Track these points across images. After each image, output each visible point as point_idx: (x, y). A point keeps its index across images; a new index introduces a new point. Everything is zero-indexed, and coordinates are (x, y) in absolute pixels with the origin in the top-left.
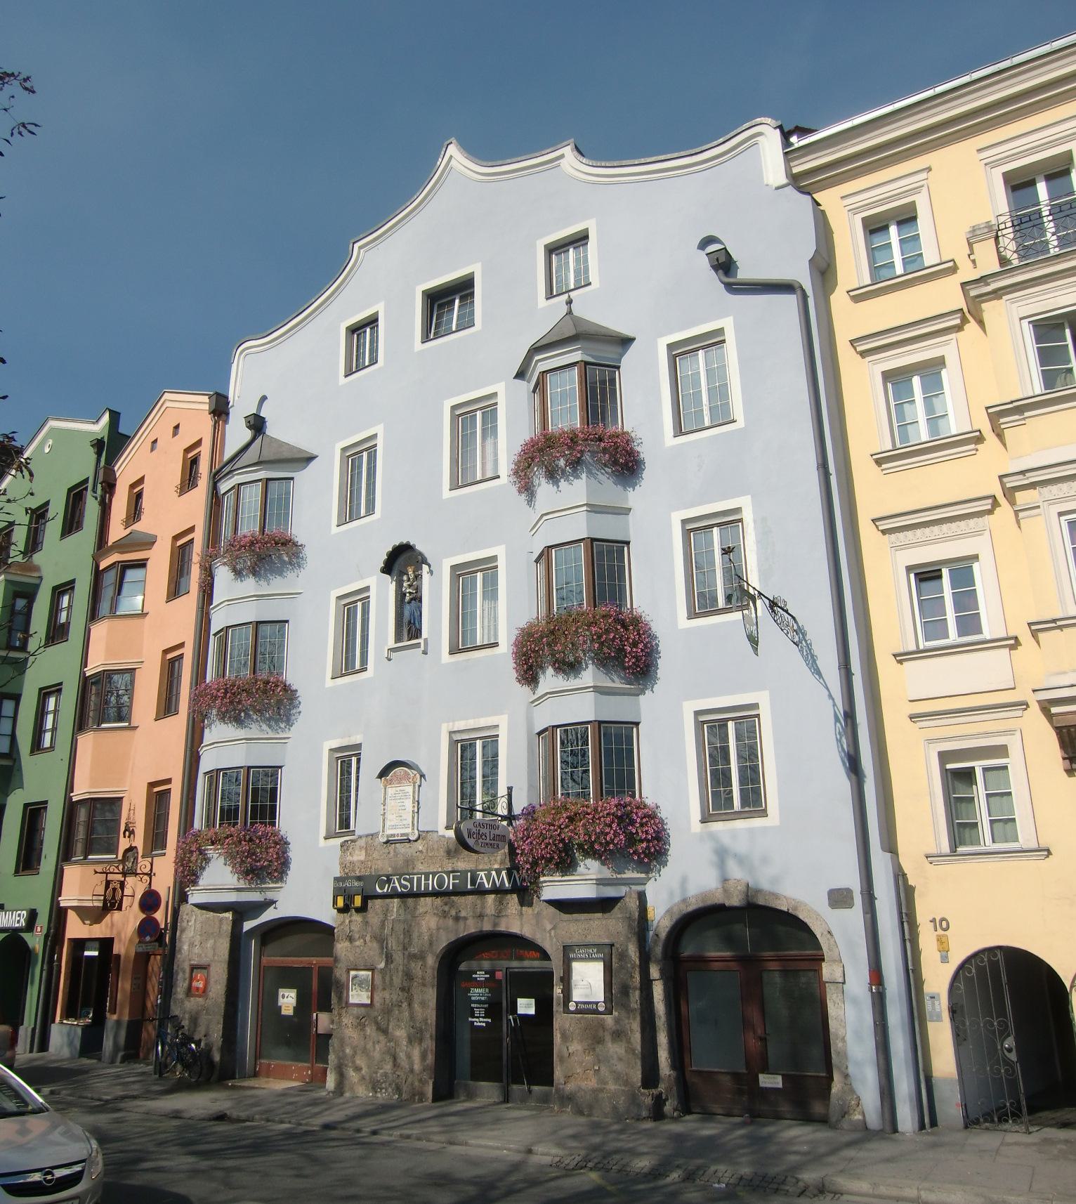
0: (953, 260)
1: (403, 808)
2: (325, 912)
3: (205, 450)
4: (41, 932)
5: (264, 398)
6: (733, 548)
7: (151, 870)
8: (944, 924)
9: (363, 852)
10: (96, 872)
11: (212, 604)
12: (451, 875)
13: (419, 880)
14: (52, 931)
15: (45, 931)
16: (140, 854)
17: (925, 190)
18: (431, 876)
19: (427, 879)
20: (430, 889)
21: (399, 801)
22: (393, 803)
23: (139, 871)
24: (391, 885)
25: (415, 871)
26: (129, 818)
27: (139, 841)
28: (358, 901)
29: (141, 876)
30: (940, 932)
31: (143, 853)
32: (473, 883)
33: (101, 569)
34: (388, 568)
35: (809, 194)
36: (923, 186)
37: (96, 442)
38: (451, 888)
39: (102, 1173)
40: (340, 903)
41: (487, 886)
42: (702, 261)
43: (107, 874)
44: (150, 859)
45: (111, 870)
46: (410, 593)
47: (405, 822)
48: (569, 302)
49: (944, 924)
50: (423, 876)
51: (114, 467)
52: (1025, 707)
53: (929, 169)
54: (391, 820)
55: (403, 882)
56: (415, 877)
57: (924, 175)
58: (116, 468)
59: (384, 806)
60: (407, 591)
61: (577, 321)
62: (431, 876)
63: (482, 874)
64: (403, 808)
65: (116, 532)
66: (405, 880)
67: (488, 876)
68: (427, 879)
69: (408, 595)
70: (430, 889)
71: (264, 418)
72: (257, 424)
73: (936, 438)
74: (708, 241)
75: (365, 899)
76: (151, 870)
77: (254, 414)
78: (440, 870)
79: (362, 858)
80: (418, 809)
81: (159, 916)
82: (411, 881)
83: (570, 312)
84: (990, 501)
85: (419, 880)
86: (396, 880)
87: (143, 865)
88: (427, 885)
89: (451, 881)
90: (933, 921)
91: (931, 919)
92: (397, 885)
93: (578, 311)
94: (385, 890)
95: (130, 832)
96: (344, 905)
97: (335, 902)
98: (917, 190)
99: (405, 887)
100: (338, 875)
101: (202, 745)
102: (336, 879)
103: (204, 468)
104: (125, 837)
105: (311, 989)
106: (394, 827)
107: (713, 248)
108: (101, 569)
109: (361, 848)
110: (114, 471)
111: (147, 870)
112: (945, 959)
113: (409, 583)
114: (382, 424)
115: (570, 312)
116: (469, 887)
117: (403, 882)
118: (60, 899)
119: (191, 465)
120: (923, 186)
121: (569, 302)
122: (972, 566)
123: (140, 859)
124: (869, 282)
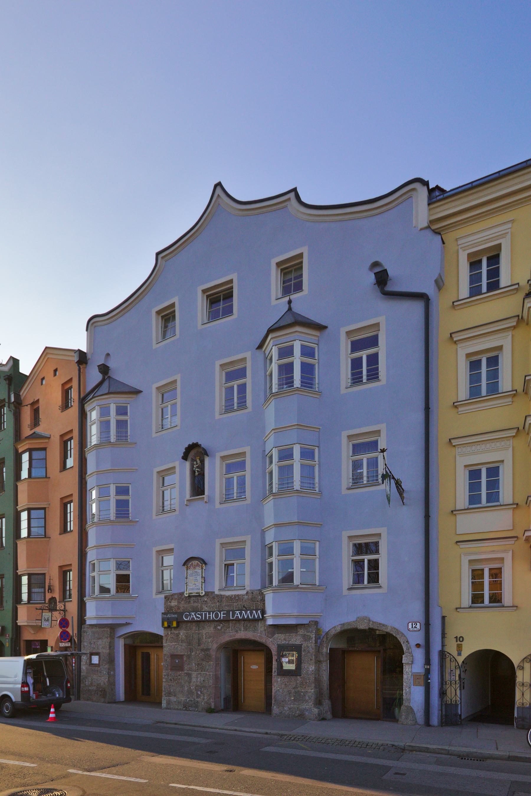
0: (518, 284)
1: (197, 580)
2: (159, 630)
3: (75, 384)
4: (8, 637)
5: (108, 355)
6: (386, 450)
7: (65, 608)
8: (461, 639)
9: (176, 601)
10: (37, 609)
11: (87, 474)
12: (222, 612)
13: (206, 615)
14: (14, 636)
15: (11, 636)
16: (58, 600)
17: (509, 236)
18: (211, 613)
19: (210, 614)
20: (211, 619)
21: (194, 577)
22: (191, 578)
23: (58, 609)
24: (191, 617)
25: (203, 610)
26: (50, 583)
27: (57, 595)
28: (175, 624)
29: (60, 611)
30: (459, 643)
31: (59, 599)
32: (233, 616)
33: (20, 452)
34: (185, 457)
35: (440, 234)
36: (508, 233)
37: (7, 377)
38: (222, 618)
39: (381, 633)
40: (166, 624)
41: (240, 618)
42: (372, 278)
43: (42, 610)
44: (63, 603)
45: (44, 608)
46: (197, 471)
47: (197, 587)
48: (290, 302)
49: (461, 639)
50: (208, 613)
51: (19, 393)
52: (516, 539)
53: (512, 221)
54: (191, 586)
55: (197, 615)
56: (204, 613)
57: (510, 225)
58: (21, 394)
59: (187, 579)
60: (196, 470)
61: (295, 314)
62: (211, 613)
63: (238, 612)
64: (197, 580)
65: (27, 431)
66: (198, 614)
67: (241, 614)
68: (210, 614)
69: (196, 472)
70: (211, 619)
71: (109, 367)
72: (104, 369)
73: (493, 394)
74: (376, 264)
75: (178, 623)
76: (65, 608)
77: (103, 364)
78: (216, 610)
79: (176, 604)
80: (204, 581)
81: (69, 630)
82: (201, 615)
83: (290, 309)
84: (515, 431)
85: (206, 615)
86: (194, 615)
87: (60, 606)
88: (210, 617)
89: (222, 615)
90: (456, 637)
91: (455, 636)
92: (194, 617)
93: (296, 308)
94: (188, 619)
95: (50, 589)
96: (168, 626)
97: (163, 624)
98: (503, 236)
99: (199, 618)
100: (163, 612)
101: (88, 548)
102: (162, 613)
103: (74, 394)
104: (49, 592)
105: (21, 704)
106: (193, 589)
107: (377, 270)
108: (20, 452)
109: (175, 599)
110: (20, 395)
111: (63, 608)
112: (459, 654)
113: (197, 465)
114: (180, 374)
115: (290, 309)
116: (231, 618)
117: (197, 615)
118: (17, 621)
119: (66, 393)
120: (508, 233)
121: (290, 302)
122: (28, 568)
123: (58, 603)
124: (467, 295)
